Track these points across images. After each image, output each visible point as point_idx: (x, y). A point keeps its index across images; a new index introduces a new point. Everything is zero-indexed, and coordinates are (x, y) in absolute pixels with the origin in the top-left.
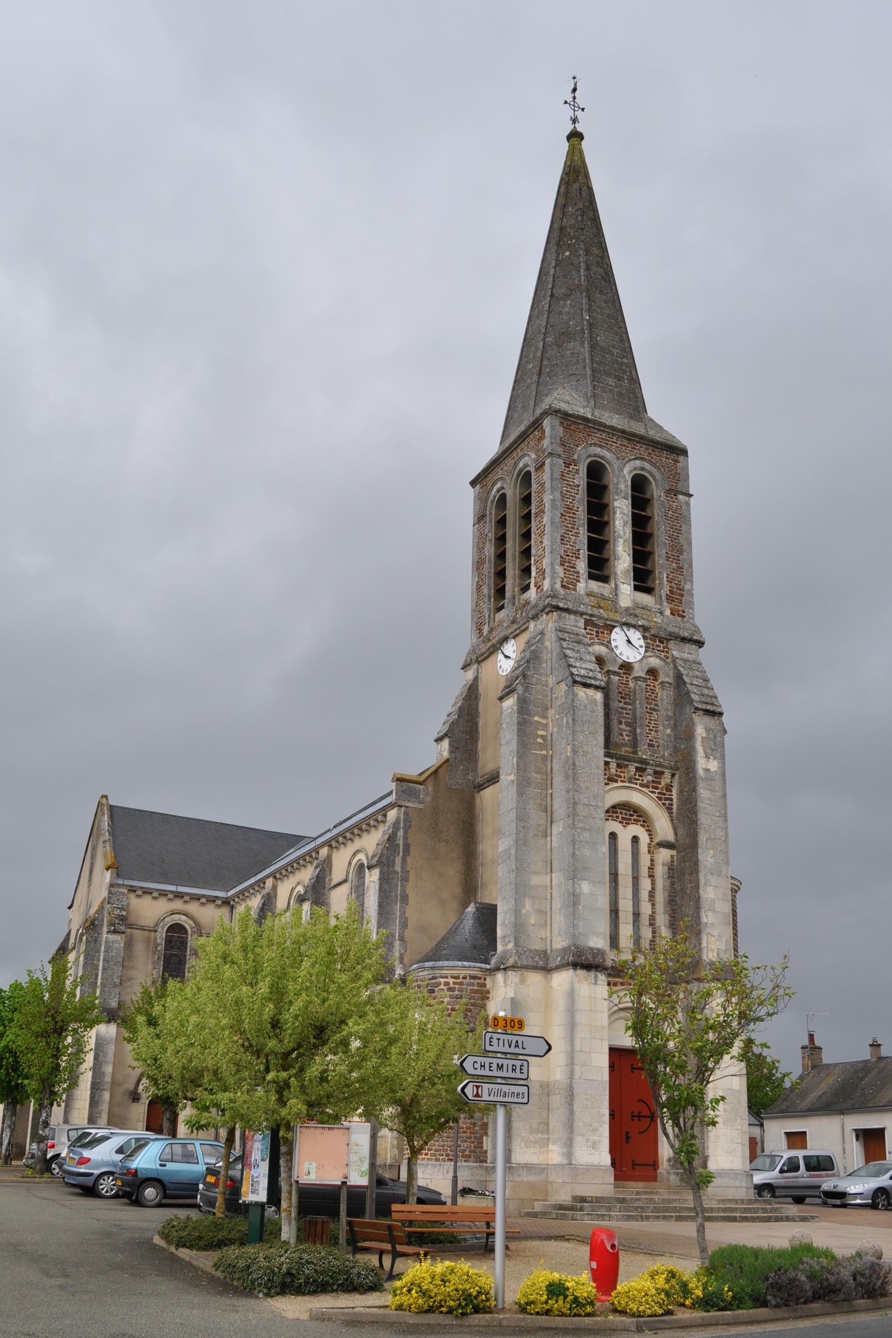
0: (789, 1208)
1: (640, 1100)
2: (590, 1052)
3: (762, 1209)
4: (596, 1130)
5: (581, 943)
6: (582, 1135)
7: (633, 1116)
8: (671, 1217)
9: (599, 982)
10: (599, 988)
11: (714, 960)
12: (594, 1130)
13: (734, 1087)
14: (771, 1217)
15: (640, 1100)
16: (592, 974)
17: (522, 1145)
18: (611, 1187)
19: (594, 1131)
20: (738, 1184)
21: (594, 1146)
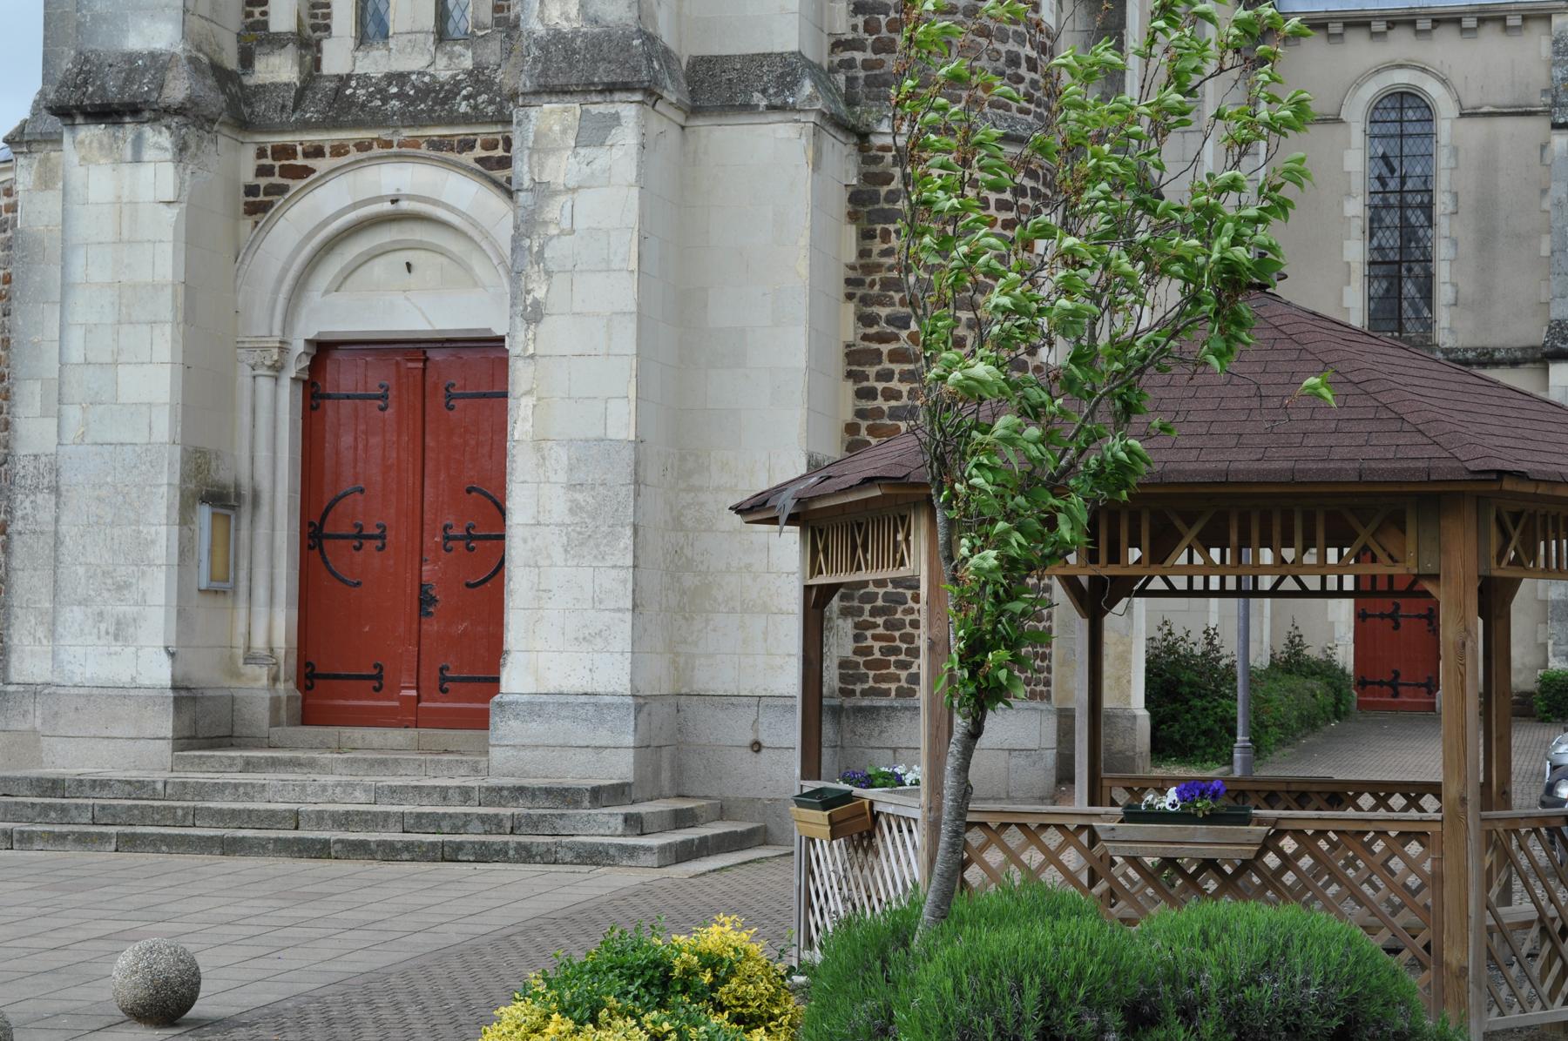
0: (589, 820)
1: (469, 491)
2: (116, 363)
3: (483, 819)
4: (127, 586)
5: (103, 43)
6: (84, 602)
7: (382, 537)
8: (103, 838)
9: (149, 154)
10: (146, 171)
11: (565, 27)
12: (122, 587)
13: (611, 434)
14: (460, 847)
15: (469, 491)
16: (129, 130)
17: (40, 634)
18: (165, 747)
19: (119, 588)
20: (603, 737)
21: (120, 632)
